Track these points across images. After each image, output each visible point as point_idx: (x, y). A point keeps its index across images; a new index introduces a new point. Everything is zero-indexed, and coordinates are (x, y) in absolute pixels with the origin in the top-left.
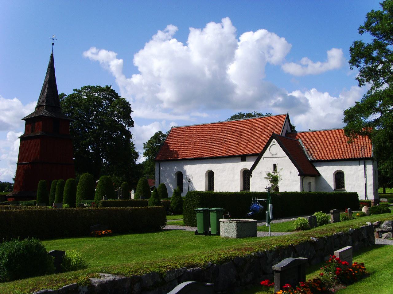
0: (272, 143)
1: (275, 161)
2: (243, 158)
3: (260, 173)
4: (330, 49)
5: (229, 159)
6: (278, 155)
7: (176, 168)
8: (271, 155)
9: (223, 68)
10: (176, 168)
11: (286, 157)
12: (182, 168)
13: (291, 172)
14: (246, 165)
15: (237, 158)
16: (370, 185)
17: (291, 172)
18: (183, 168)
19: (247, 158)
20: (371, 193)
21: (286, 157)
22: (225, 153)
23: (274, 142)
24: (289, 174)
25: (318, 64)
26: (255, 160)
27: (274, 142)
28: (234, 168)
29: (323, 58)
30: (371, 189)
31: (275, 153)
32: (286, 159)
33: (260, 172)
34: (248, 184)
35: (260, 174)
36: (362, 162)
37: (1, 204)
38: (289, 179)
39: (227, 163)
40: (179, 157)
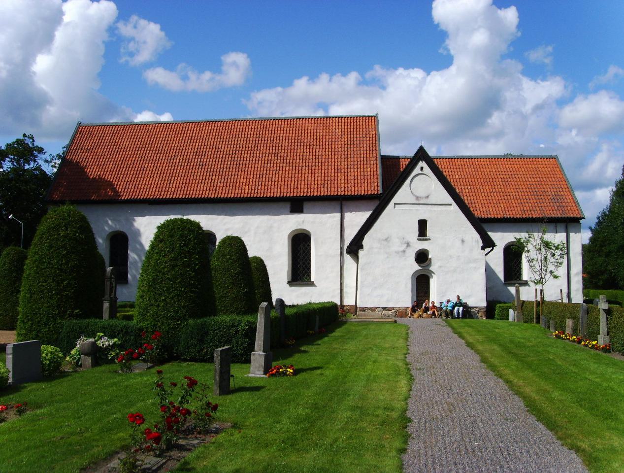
0: (417, 170)
1: (423, 213)
2: (297, 205)
3: (386, 240)
4: (226, 52)
5: (221, 205)
6: (432, 200)
7: (110, 222)
8: (414, 197)
9: (27, 61)
10: (110, 222)
11: (451, 205)
12: (130, 222)
13: (463, 241)
14: (303, 221)
15: (281, 204)
16: (577, 274)
17: (463, 241)
18: (132, 225)
19: (306, 206)
20: (577, 290)
21: (451, 205)
22: (247, 191)
23: (422, 169)
24: (458, 243)
25: (207, 75)
26: (374, 208)
27: (422, 169)
28: (271, 227)
29: (217, 67)
30: (577, 282)
31: (424, 194)
32: (451, 211)
33: (386, 237)
34: (306, 266)
35: (385, 243)
36: (561, 226)
37: (3, 433)
38: (459, 256)
39: (252, 215)
40: (120, 196)
